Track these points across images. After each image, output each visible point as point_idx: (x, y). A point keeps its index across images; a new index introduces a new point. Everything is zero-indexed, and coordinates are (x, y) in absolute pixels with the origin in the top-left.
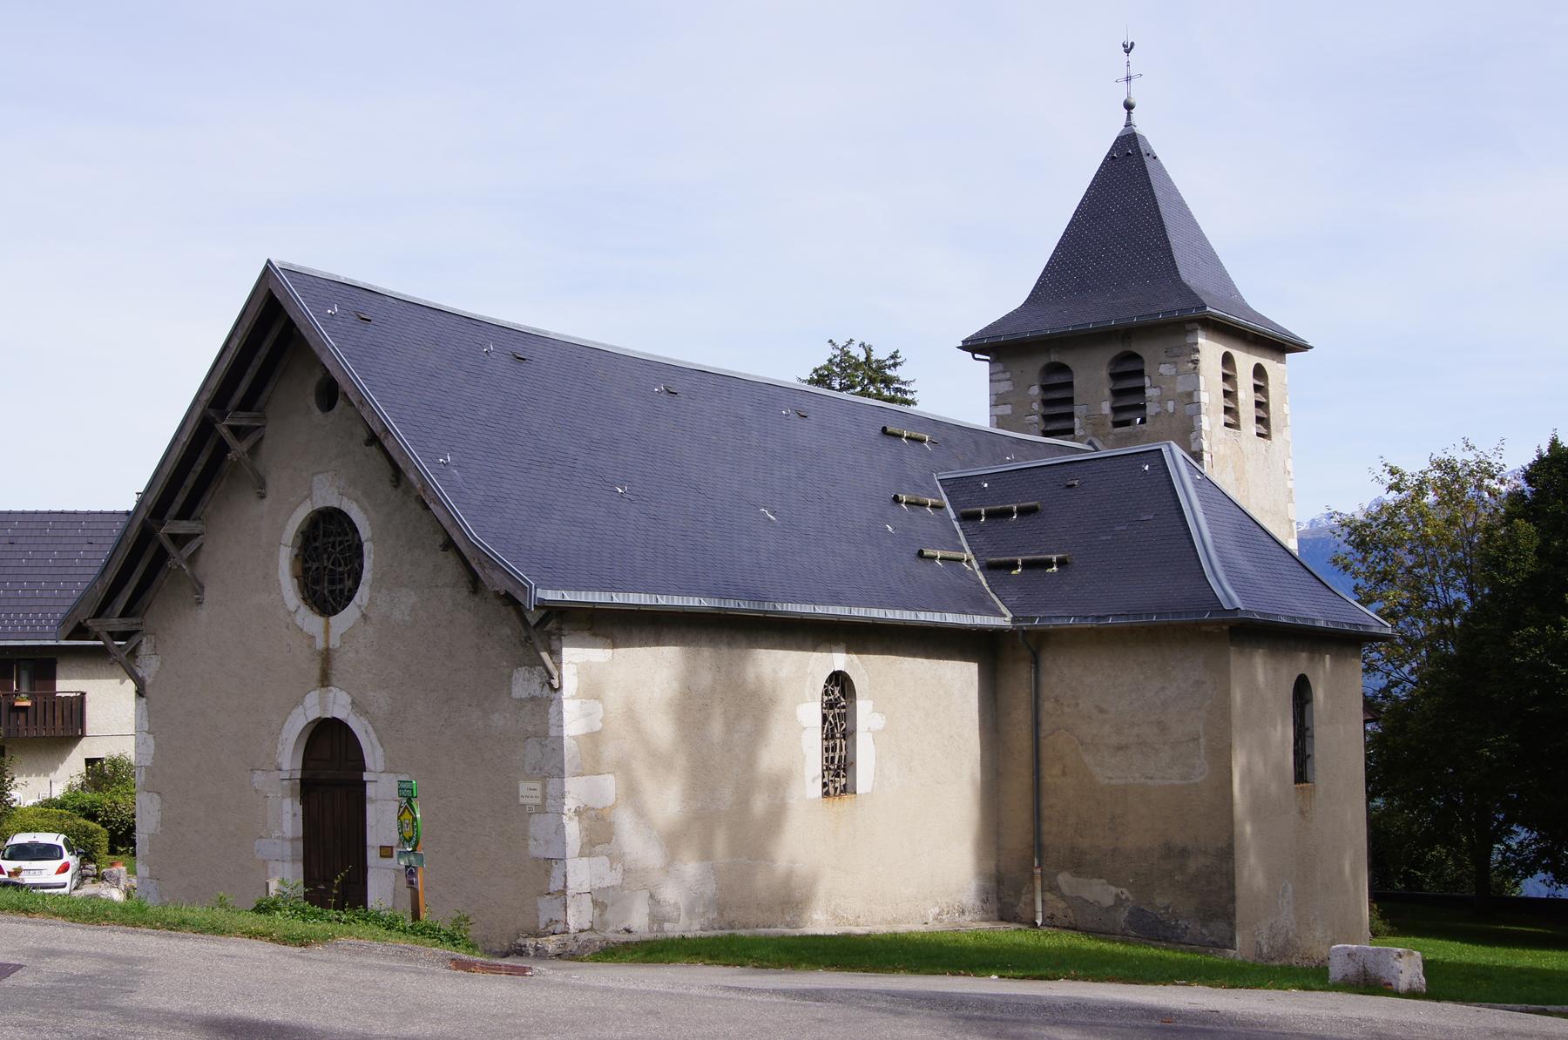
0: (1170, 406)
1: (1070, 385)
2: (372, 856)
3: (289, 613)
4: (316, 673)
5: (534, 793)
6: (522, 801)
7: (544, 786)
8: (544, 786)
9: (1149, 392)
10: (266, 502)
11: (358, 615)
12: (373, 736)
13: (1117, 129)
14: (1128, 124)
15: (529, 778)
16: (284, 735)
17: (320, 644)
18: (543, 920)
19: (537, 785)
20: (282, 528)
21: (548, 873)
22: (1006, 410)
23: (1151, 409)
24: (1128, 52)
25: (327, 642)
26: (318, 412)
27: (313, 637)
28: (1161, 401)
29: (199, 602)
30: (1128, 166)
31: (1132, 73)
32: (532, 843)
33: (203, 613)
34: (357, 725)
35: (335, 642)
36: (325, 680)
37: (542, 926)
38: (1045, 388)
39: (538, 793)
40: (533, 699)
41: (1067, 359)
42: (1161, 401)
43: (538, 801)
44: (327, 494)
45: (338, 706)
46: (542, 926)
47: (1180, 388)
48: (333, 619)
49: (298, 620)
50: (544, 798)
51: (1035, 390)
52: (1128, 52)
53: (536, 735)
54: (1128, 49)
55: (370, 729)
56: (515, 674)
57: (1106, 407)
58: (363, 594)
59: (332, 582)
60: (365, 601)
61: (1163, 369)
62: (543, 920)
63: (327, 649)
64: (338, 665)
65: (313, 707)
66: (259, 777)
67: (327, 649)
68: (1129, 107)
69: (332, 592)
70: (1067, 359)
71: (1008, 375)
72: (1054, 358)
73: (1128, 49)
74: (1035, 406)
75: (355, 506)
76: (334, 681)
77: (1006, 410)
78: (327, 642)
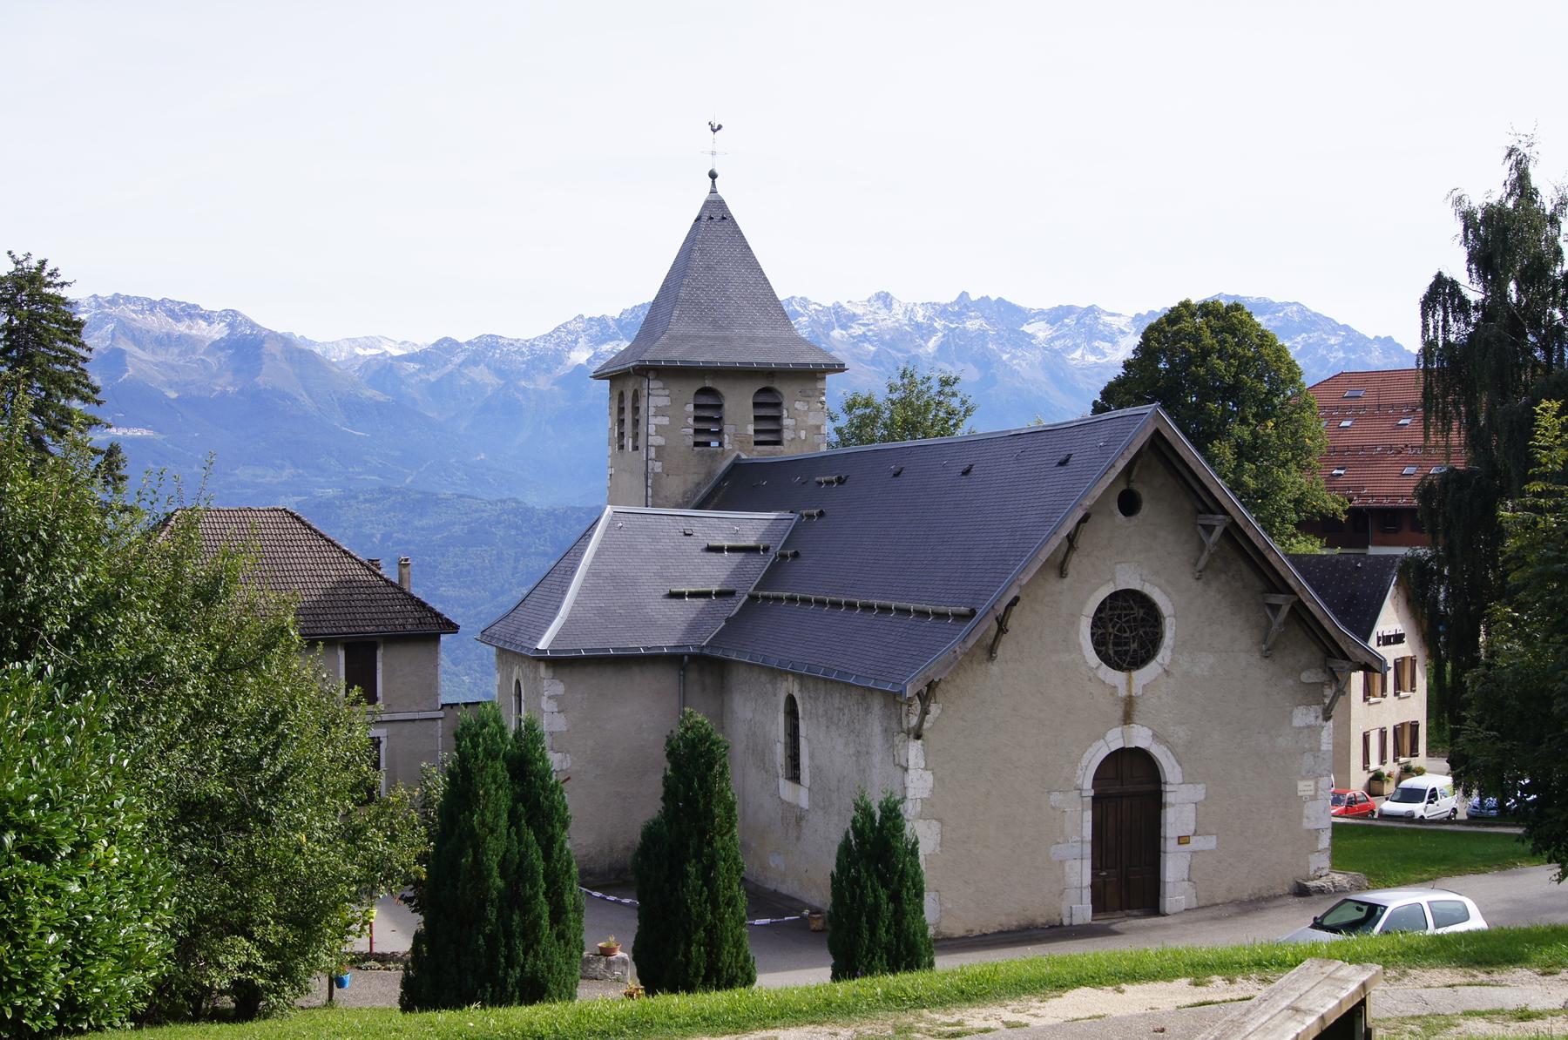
0: (803, 434)
1: (719, 407)
2: (1170, 846)
4: (1119, 713)
9: (786, 422)
10: (1067, 581)
11: (1160, 670)
13: (704, 194)
14: (714, 191)
15: (1303, 778)
16: (1084, 763)
17: (1122, 692)
18: (1312, 868)
19: (1312, 783)
20: (1083, 603)
23: (787, 435)
25: (1129, 690)
26: (1120, 516)
28: (796, 429)
30: (715, 218)
33: (994, 668)
34: (1158, 752)
35: (1137, 690)
36: (1127, 718)
38: (696, 406)
40: (1309, 727)
42: (796, 429)
44: (1128, 578)
45: (1140, 737)
48: (1135, 674)
49: (1100, 674)
51: (690, 408)
53: (1311, 750)
56: (1296, 711)
57: (751, 429)
58: (1164, 655)
59: (1115, 644)
60: (1167, 661)
61: (798, 405)
62: (1312, 868)
63: (1130, 696)
64: (1140, 707)
65: (1115, 740)
66: (1056, 798)
68: (713, 176)
70: (721, 387)
72: (708, 384)
74: (691, 421)
75: (1157, 590)
76: (1135, 718)
78: (1129, 690)
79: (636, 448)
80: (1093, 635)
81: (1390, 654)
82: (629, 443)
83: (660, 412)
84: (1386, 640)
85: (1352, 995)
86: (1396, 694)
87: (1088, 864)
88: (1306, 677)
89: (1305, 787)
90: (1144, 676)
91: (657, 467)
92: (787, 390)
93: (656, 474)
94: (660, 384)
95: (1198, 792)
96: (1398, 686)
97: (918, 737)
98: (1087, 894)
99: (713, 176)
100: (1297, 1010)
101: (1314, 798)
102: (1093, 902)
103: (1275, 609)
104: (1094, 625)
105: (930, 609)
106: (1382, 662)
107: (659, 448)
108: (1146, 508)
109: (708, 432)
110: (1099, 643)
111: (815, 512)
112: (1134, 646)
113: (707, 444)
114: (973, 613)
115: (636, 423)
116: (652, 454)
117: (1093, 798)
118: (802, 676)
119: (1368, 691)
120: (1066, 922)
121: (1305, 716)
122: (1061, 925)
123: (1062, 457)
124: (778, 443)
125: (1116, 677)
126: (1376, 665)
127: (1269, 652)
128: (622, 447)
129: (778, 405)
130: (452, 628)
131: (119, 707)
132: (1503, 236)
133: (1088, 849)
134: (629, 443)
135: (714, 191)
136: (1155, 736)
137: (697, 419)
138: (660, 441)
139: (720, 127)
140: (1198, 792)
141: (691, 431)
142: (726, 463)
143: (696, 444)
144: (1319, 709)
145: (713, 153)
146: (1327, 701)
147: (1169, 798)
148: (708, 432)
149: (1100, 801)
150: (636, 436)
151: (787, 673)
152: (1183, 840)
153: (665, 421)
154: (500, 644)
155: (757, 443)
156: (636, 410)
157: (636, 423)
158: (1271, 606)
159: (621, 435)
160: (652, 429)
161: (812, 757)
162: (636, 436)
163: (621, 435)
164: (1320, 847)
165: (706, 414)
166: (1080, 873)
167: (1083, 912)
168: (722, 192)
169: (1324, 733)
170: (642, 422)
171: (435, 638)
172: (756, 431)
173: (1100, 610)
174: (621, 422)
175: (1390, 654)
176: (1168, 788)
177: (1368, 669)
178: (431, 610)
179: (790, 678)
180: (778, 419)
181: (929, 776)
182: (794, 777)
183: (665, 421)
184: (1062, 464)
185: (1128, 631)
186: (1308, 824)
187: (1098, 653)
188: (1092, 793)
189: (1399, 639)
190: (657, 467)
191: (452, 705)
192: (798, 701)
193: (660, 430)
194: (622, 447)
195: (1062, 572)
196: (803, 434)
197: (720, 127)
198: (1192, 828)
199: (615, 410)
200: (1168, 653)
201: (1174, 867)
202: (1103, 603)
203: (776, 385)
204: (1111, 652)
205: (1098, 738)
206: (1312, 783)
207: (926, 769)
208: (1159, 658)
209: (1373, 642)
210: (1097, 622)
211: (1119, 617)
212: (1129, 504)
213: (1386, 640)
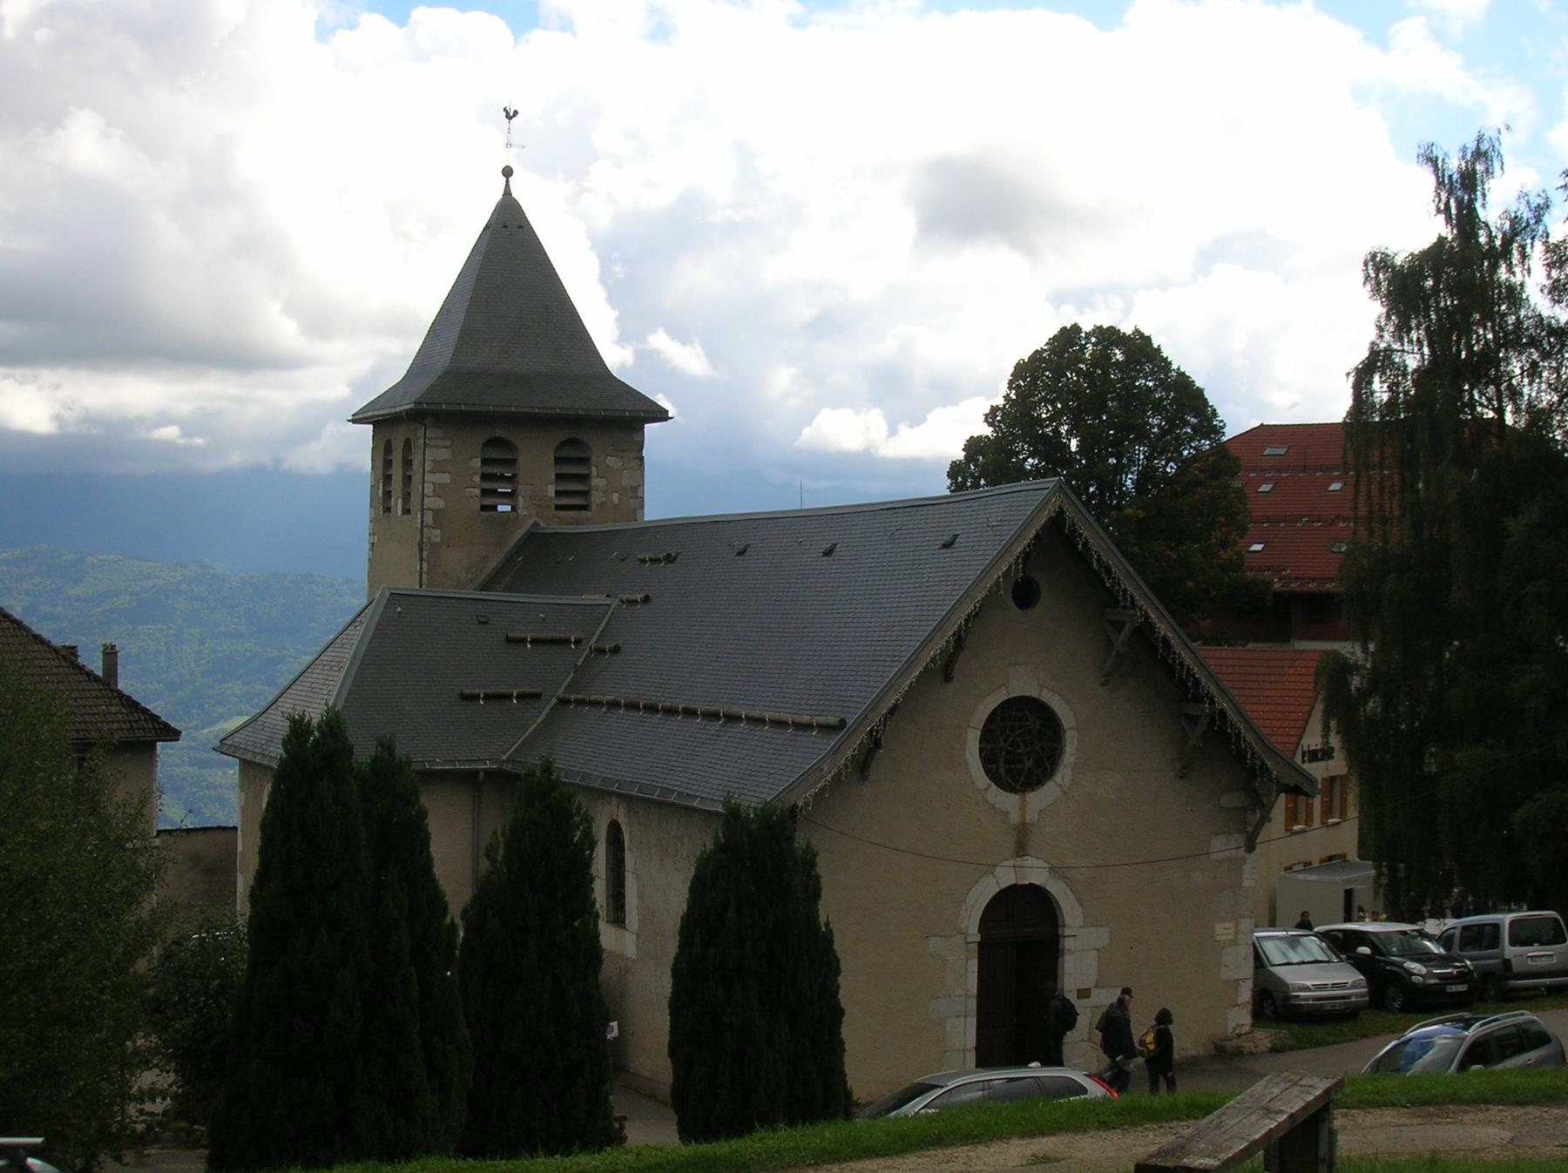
0: (615, 497)
1: (512, 462)
7: (1237, 927)
8: (1237, 927)
9: (595, 482)
14: (507, 192)
16: (970, 902)
17: (1015, 818)
18: (1231, 1024)
19: (1231, 925)
23: (596, 498)
24: (509, 117)
26: (1016, 609)
31: (513, 141)
34: (1057, 889)
35: (1032, 816)
36: (1021, 850)
38: (485, 462)
40: (1229, 859)
44: (1023, 684)
45: (1036, 873)
47: (626, 482)
48: (1030, 796)
49: (990, 798)
51: (477, 462)
57: (551, 490)
58: (1063, 775)
59: (1007, 762)
60: (1067, 781)
61: (610, 461)
62: (1231, 1024)
63: (1024, 823)
65: (1006, 877)
66: (935, 943)
67: (1024, 823)
68: (508, 172)
69: (1008, 771)
71: (448, 443)
72: (499, 433)
73: (510, 115)
74: (477, 479)
75: (1056, 697)
78: (1023, 816)
79: (407, 511)
80: (981, 750)
81: (1318, 770)
82: (397, 504)
83: (439, 467)
84: (1313, 756)
85: (1317, 1098)
86: (1324, 824)
87: (972, 1022)
90: (1041, 798)
91: (435, 535)
92: (597, 444)
93: (434, 545)
94: (440, 433)
95: (1101, 936)
96: (1327, 813)
99: (508, 172)
100: (1269, 1111)
103: (1193, 720)
104: (983, 739)
105: (767, 716)
106: (1311, 780)
107: (437, 513)
108: (1045, 600)
109: (494, 493)
110: (988, 761)
111: (639, 597)
112: (1029, 763)
113: (494, 508)
114: (843, 723)
115: (407, 480)
116: (429, 519)
117: (980, 944)
118: (630, 797)
119: (1292, 818)
121: (1223, 846)
123: (947, 538)
124: (585, 508)
125: (1007, 801)
126: (1306, 787)
127: (1185, 770)
128: (388, 509)
129: (585, 461)
130: (172, 734)
132: (1449, 290)
134: (397, 504)
135: (507, 192)
137: (485, 477)
138: (440, 503)
139: (516, 113)
140: (1101, 936)
141: (478, 492)
142: (520, 533)
143: (484, 508)
144: (1240, 840)
146: (1250, 829)
147: (1068, 944)
148: (494, 493)
149: (987, 949)
150: (407, 497)
151: (611, 794)
153: (445, 478)
154: (248, 756)
155: (558, 508)
156: (408, 464)
157: (407, 480)
158: (1187, 717)
159: (387, 494)
160: (429, 489)
161: (641, 896)
162: (407, 497)
163: (387, 494)
165: (497, 470)
168: (516, 194)
169: (1247, 868)
170: (416, 479)
171: (151, 747)
172: (557, 493)
173: (991, 720)
174: (387, 479)
175: (1318, 770)
176: (1067, 932)
177: (1295, 791)
178: (145, 711)
179: (614, 800)
180: (584, 478)
182: (618, 919)
183: (445, 478)
184: (947, 546)
185: (1022, 746)
186: (1226, 974)
187: (987, 771)
188: (978, 938)
189: (1327, 754)
190: (435, 535)
191: (169, 832)
192: (624, 828)
193: (439, 490)
194: (388, 509)
195: (948, 678)
196: (615, 497)
197: (516, 113)
198: (1093, 978)
199: (380, 464)
200: (1069, 772)
202: (994, 712)
203: (582, 436)
204: (1002, 771)
208: (1057, 778)
209: (1298, 759)
210: (987, 735)
211: (1012, 730)
212: (1025, 594)
213: (1313, 756)
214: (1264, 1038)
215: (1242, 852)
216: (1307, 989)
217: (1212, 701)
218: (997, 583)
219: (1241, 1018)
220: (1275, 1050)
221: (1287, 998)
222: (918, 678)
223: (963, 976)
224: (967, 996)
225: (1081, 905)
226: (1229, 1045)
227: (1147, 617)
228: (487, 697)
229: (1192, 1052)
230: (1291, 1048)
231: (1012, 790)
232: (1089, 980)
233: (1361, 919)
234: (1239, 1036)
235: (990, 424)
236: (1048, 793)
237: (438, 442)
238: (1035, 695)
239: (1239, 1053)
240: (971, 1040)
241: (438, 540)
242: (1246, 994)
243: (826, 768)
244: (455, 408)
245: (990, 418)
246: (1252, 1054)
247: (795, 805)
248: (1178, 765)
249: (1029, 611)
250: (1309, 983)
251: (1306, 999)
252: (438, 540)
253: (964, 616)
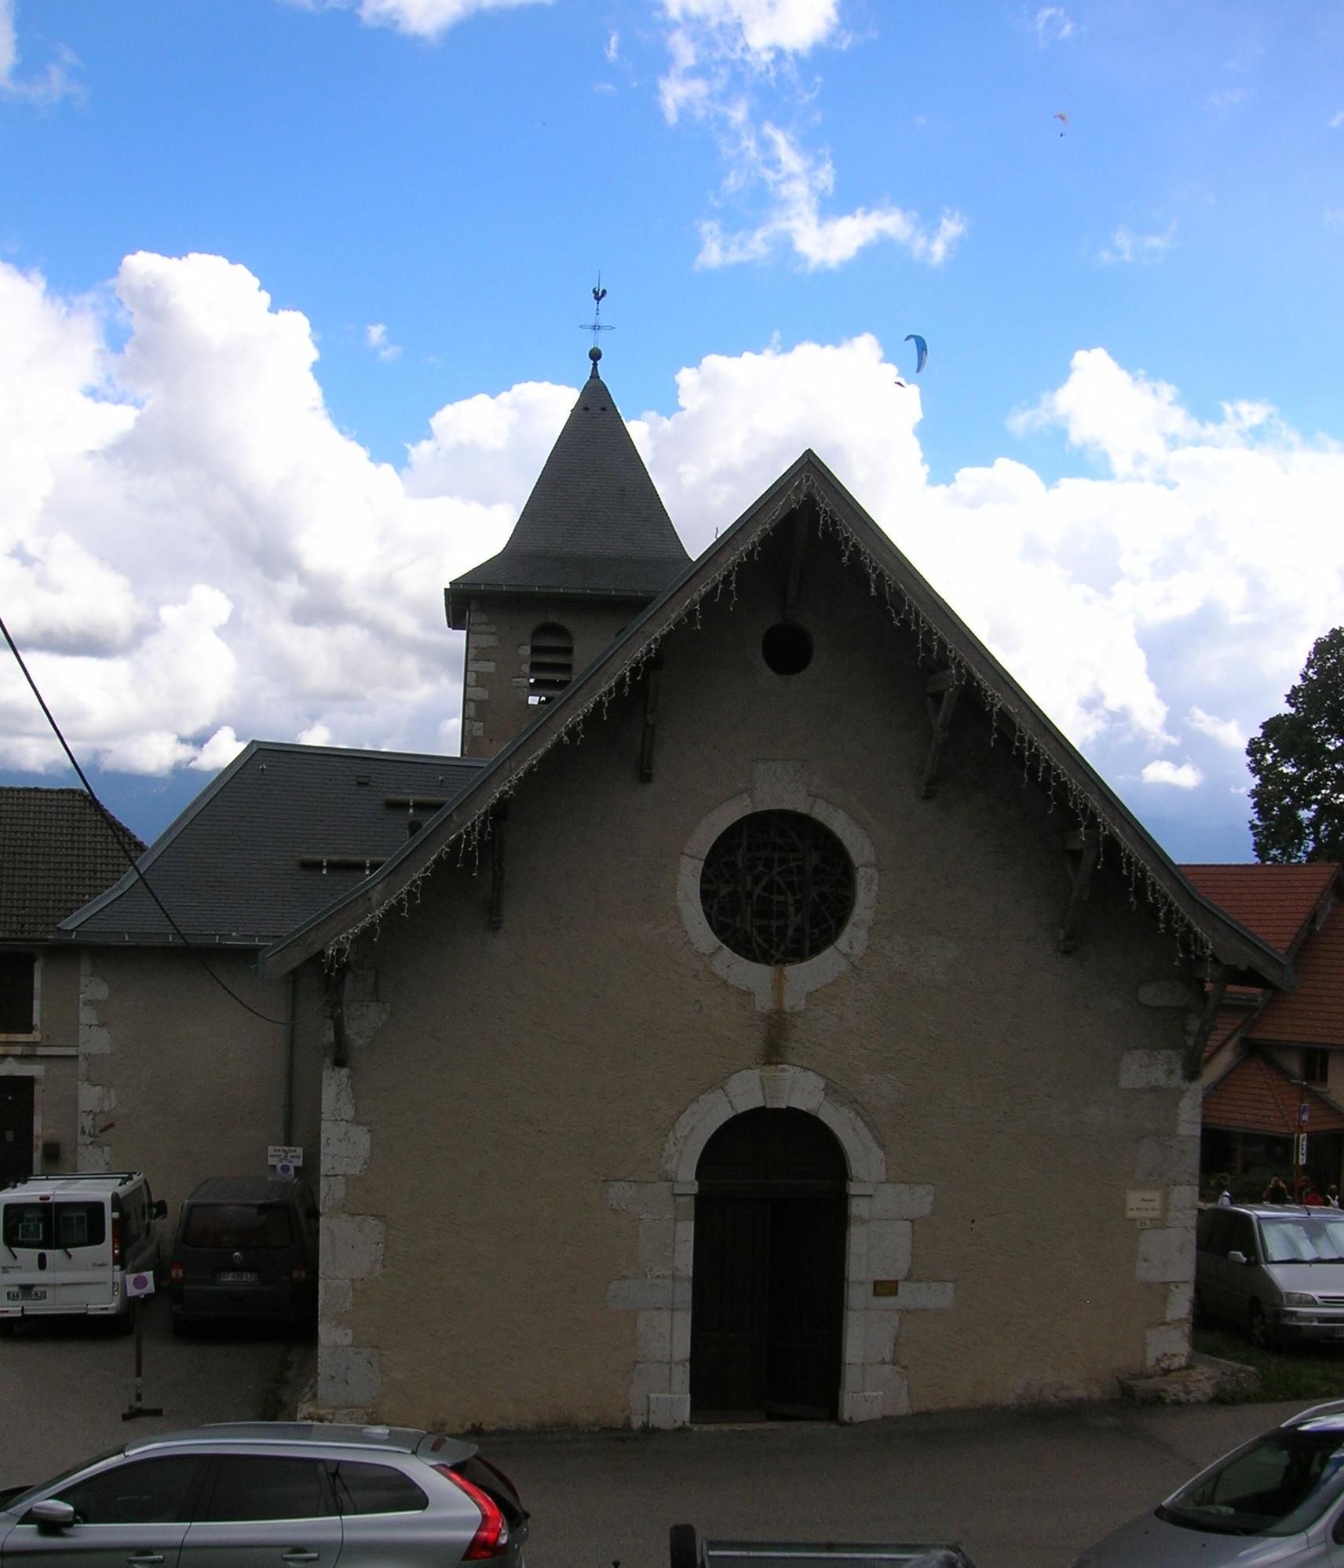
1: (568, 651)
2: (857, 1296)
3: (700, 956)
5: (1150, 1205)
6: (1130, 1214)
7: (1166, 1196)
8: (1166, 1196)
12: (866, 1134)
14: (595, 375)
17: (764, 1003)
18: (1153, 1353)
19: (1156, 1196)
21: (1164, 1300)
22: (489, 667)
24: (598, 299)
27: (749, 994)
29: (495, 926)
32: (1141, 1265)
35: (793, 1001)
36: (773, 1052)
37: (1150, 1362)
38: (535, 650)
39: (1157, 1204)
40: (1154, 1090)
41: (570, 624)
43: (1156, 1214)
44: (780, 790)
45: (799, 1090)
46: (1150, 1362)
48: (791, 970)
50: (1166, 1208)
51: (526, 650)
52: (598, 299)
54: (599, 296)
55: (860, 1124)
58: (853, 938)
60: (859, 950)
62: (1153, 1353)
63: (780, 1012)
65: (747, 1092)
68: (595, 355)
72: (552, 618)
73: (599, 296)
77: (489, 667)
78: (779, 1000)
80: (704, 895)
88: (1148, 994)
89: (1141, 1203)
94: (485, 618)
95: (920, 1200)
97: (340, 1062)
98: (682, 1377)
99: (595, 355)
101: (1161, 1224)
102: (693, 1391)
117: (698, 1198)
120: (637, 1423)
122: (628, 1426)
127: (1073, 943)
131: (87, 1016)
133: (686, 1293)
135: (595, 375)
136: (831, 1090)
137: (535, 667)
139: (604, 292)
140: (920, 1200)
145: (596, 328)
146: (1191, 1042)
147: (857, 1208)
152: (885, 1288)
164: (1170, 1316)
166: (672, 1336)
167: (670, 1400)
181: (362, 1138)
186: (1145, 1272)
188: (694, 1188)
197: (604, 292)
198: (903, 1264)
200: (862, 934)
201: (865, 1337)
205: (710, 1087)
206: (1156, 1196)
207: (356, 1121)
208: (842, 942)
214: (1205, 1378)
215: (1177, 1080)
216: (1312, 1303)
217: (1093, 824)
218: (691, 613)
219: (1172, 1343)
220: (1220, 1400)
221: (1279, 1314)
222: (543, 760)
223: (670, 1249)
224: (674, 1278)
225: (883, 1147)
226: (1142, 1385)
227: (971, 677)
228: (332, 866)
229: (1080, 1393)
230: (1248, 1399)
231: (764, 957)
232: (897, 1266)
233: (74, 1172)
234: (1167, 1371)
235: (1292, 705)
236: (824, 966)
237: (483, 628)
238: (802, 809)
239: (1155, 1401)
240: (682, 1346)
241: (480, 733)
242: (1181, 1304)
243: (375, 896)
244: (499, 589)
245: (1291, 699)
246: (1178, 1403)
247: (322, 953)
248: (1062, 933)
249: (794, 678)
250: (1315, 1294)
251: (1310, 1318)
252: (480, 733)
253: (629, 664)
